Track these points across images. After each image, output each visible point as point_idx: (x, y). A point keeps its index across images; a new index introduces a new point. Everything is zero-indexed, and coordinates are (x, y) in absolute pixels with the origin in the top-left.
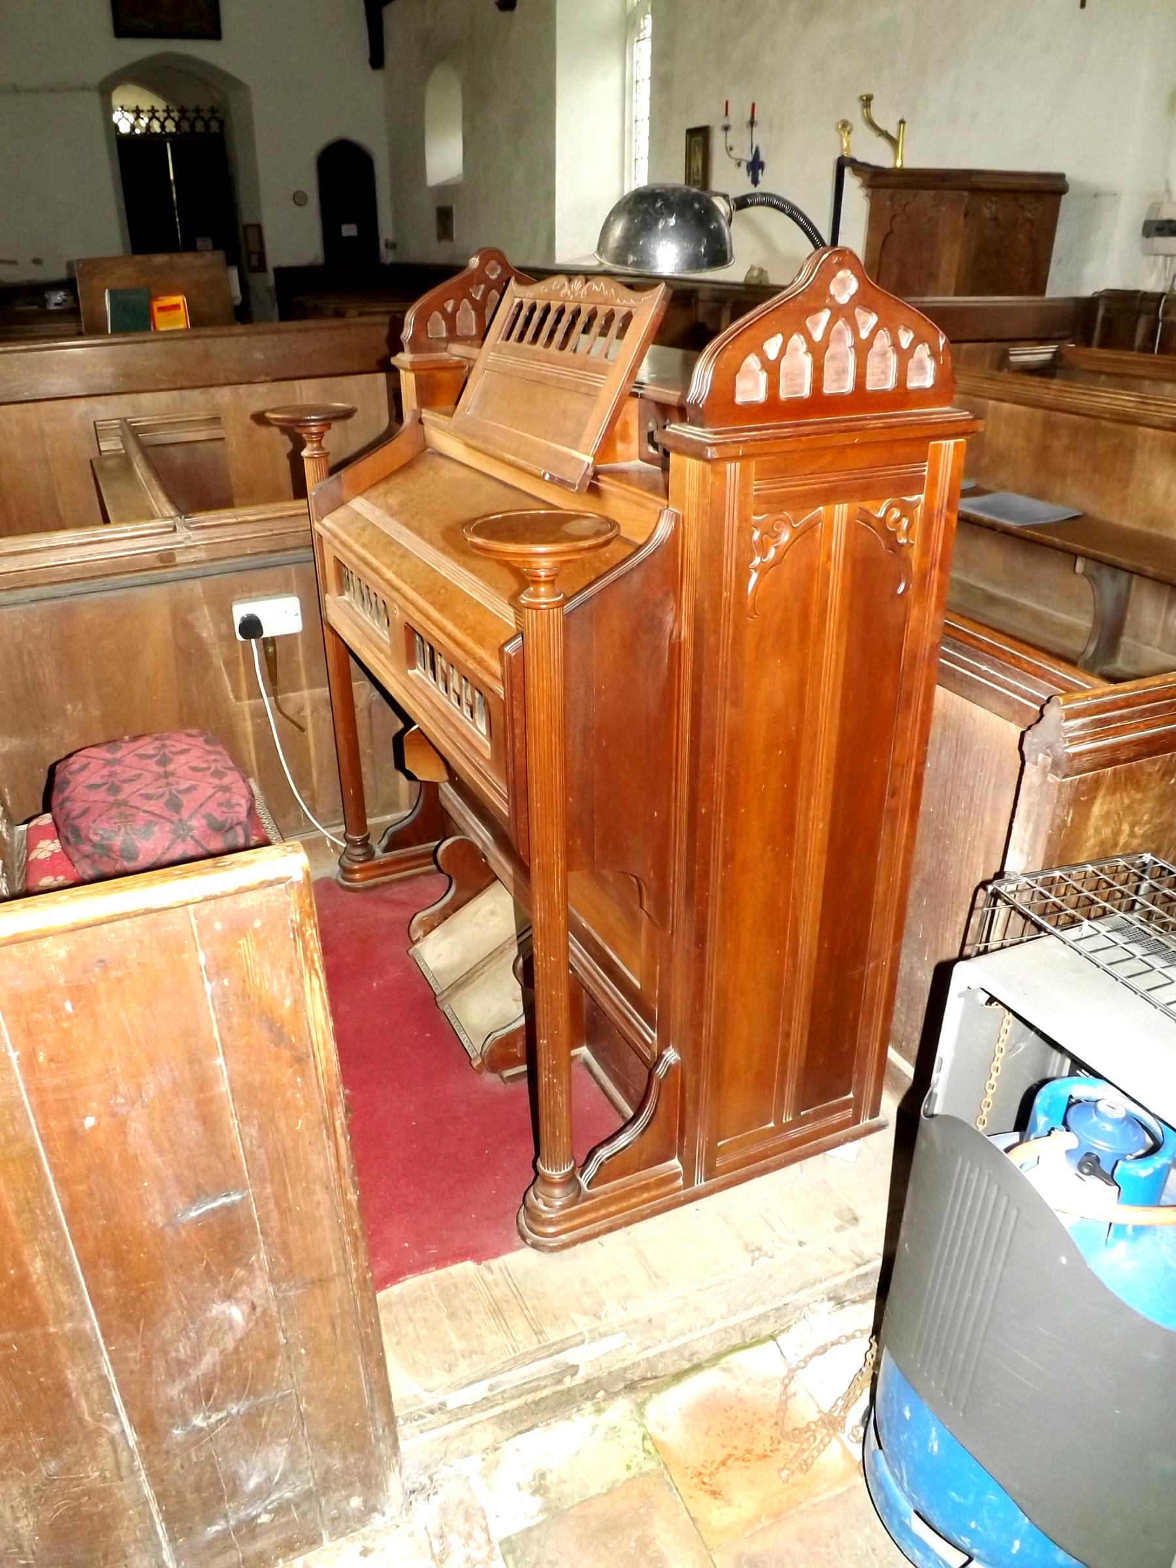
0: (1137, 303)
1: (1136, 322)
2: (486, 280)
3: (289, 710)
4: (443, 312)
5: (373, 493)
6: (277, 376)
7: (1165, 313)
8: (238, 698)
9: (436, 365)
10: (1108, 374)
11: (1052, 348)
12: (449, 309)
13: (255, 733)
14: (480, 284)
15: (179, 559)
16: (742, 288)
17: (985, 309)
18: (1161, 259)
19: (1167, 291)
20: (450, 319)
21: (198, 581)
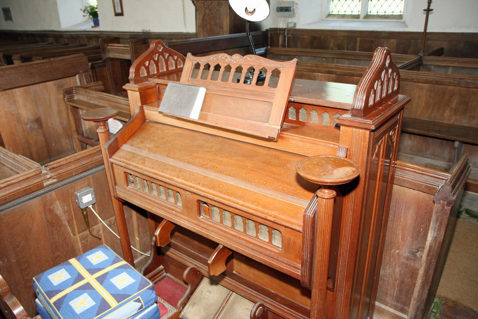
0: (278, 31)
1: (279, 38)
2: (158, 52)
3: (94, 233)
4: (145, 66)
5: (130, 141)
6: (4, 89)
7: (287, 34)
8: (74, 235)
9: (146, 88)
10: (284, 55)
11: (265, 48)
12: (147, 65)
13: (82, 247)
14: (156, 53)
15: (45, 184)
16: (142, 34)
17: (240, 37)
18: (283, 18)
19: (287, 27)
20: (147, 68)
21: (53, 192)
